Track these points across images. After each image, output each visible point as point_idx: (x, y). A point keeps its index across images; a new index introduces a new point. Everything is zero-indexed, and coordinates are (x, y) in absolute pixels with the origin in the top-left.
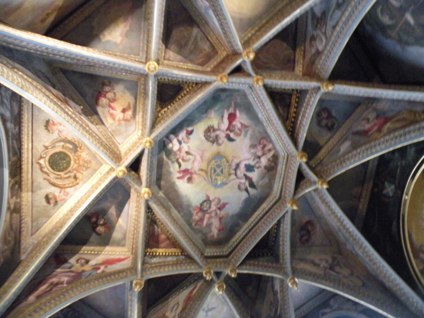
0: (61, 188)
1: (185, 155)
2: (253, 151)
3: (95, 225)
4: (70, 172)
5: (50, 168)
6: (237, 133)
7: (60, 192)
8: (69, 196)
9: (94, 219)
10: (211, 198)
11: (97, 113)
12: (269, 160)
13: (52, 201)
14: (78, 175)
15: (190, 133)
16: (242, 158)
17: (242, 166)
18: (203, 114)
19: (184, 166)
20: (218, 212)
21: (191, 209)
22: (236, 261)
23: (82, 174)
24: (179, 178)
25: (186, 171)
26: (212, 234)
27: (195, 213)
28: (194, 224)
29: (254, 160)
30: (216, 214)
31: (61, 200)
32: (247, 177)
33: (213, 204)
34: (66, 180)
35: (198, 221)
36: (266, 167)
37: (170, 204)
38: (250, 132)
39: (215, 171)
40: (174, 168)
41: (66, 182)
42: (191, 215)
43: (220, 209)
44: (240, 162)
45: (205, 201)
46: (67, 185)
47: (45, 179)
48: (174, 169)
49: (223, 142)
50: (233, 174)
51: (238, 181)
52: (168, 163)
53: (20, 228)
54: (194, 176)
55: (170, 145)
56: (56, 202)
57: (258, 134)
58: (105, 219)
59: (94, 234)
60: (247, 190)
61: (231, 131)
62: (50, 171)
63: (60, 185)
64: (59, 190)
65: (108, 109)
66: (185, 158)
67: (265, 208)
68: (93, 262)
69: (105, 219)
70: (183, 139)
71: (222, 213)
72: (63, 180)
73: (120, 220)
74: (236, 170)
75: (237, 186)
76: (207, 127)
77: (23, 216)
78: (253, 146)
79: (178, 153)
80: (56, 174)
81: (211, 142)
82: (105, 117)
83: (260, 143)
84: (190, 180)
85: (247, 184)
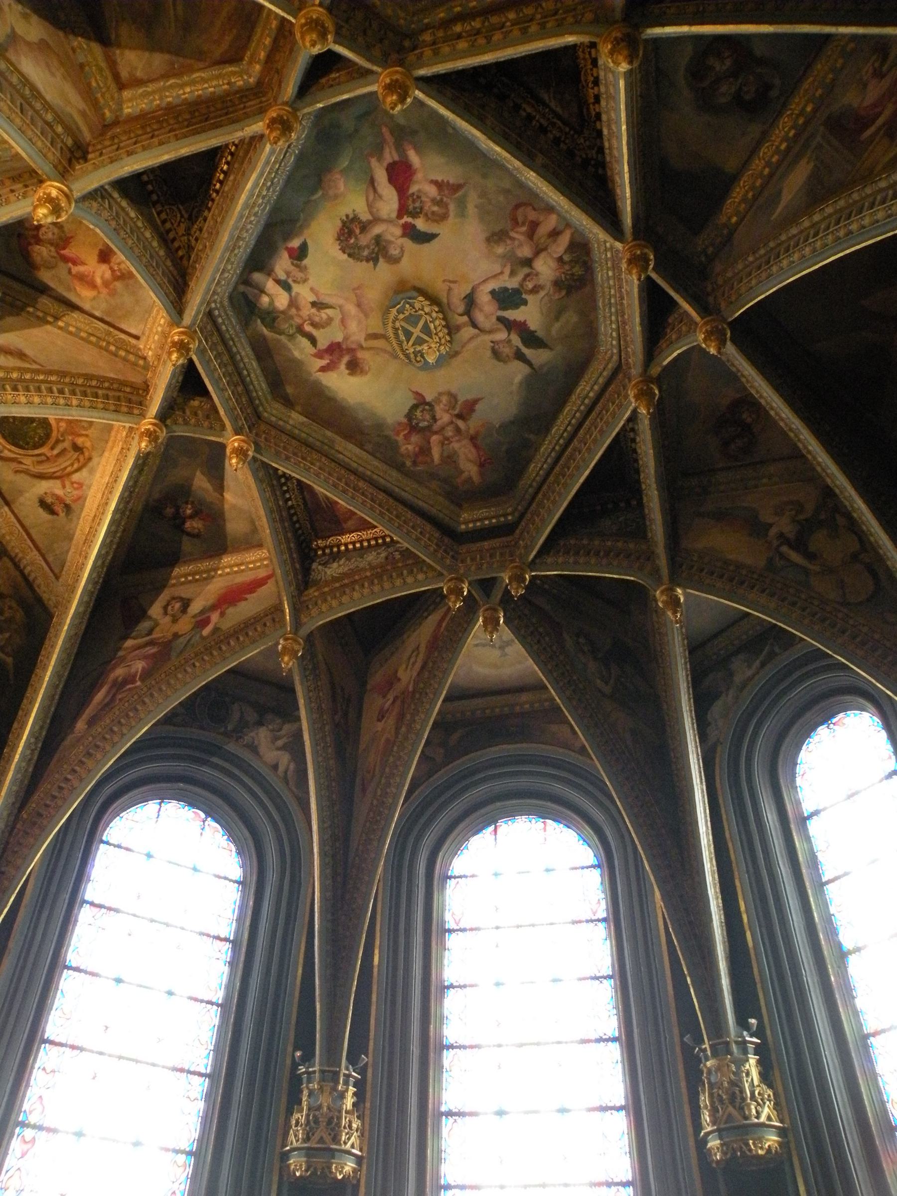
0: (61, 477)
1: (314, 310)
2: (500, 250)
3: (178, 522)
4: (58, 441)
5: (13, 448)
6: (433, 213)
7: (64, 487)
8: (84, 487)
9: (169, 511)
10: (429, 399)
11: (44, 289)
12: (560, 260)
13: (58, 508)
14: (80, 441)
15: (300, 254)
16: (475, 277)
17: (484, 298)
18: (313, 191)
19: (324, 338)
20: (460, 423)
21: (388, 433)
22: (528, 548)
23: (87, 436)
24: (323, 369)
25: (334, 349)
26: (466, 475)
27: (400, 438)
28: (408, 463)
29: (513, 273)
30: (458, 430)
31: (75, 501)
32: (509, 325)
33: (438, 409)
34: (61, 460)
35: (416, 455)
36: (557, 284)
37: (329, 433)
38: (473, 200)
39: (408, 335)
40: (301, 349)
41: (64, 462)
42: (393, 446)
43: (460, 416)
44: (474, 290)
45: (415, 407)
46: (69, 469)
47: (16, 472)
48: (302, 351)
49: (402, 251)
50: (465, 325)
51: (487, 338)
52: (279, 341)
53: (25, 578)
54: (360, 354)
55: (265, 300)
56: (68, 508)
57: (501, 198)
58: (193, 503)
59: (185, 538)
60: (519, 356)
61: (415, 215)
62: (20, 454)
63: (54, 473)
64: (58, 483)
65: (62, 268)
66: (317, 319)
67: (587, 396)
68: (196, 607)
69: (193, 503)
70: (288, 274)
71: (473, 424)
72: (55, 461)
73: (228, 496)
74: (468, 312)
75: (489, 353)
76: (339, 224)
77: (17, 555)
78: (496, 237)
79: (293, 311)
80: (32, 456)
81: (368, 260)
82: (69, 289)
83: (516, 223)
84: (354, 367)
85: (516, 340)
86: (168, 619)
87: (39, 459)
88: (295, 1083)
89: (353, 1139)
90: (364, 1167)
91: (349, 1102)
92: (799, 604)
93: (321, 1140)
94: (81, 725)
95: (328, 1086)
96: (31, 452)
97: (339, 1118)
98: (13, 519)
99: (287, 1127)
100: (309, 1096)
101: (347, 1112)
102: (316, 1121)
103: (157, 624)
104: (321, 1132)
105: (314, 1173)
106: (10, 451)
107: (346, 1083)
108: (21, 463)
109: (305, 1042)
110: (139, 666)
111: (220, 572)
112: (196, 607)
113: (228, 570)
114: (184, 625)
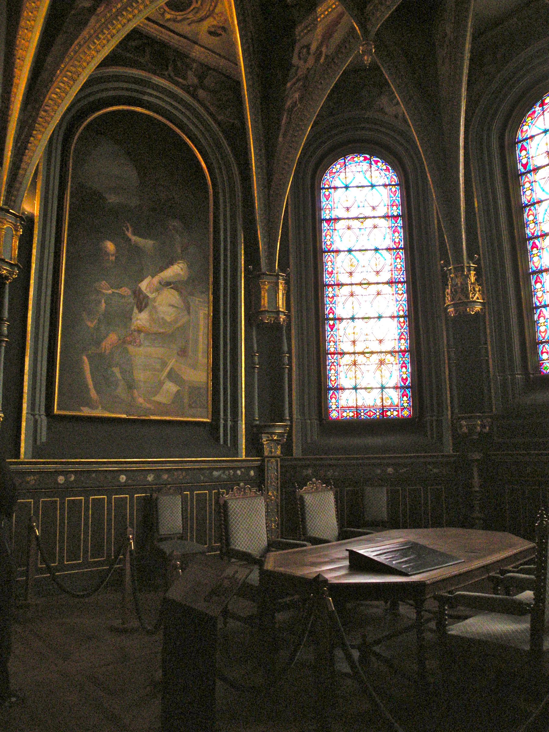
0: (211, 14)
5: (180, 13)
7: (215, 18)
13: (219, 31)
56: (224, 29)
68: (313, 47)
86: (302, 62)
87: (195, 11)
88: (445, 276)
89: (477, 295)
90: (487, 307)
91: (473, 279)
92: (374, 11)
93: (460, 299)
94: (280, 139)
95: (459, 274)
96: (189, 10)
97: (467, 287)
98: (203, 49)
99: (444, 296)
100: (452, 280)
101: (472, 284)
102: (456, 291)
103: (298, 68)
104: (459, 295)
105: (459, 314)
106: (180, 15)
107: (469, 270)
108: (188, 19)
109: (444, 255)
110: (297, 95)
111: (319, 20)
112: (313, 47)
113: (322, 16)
114: (311, 61)
